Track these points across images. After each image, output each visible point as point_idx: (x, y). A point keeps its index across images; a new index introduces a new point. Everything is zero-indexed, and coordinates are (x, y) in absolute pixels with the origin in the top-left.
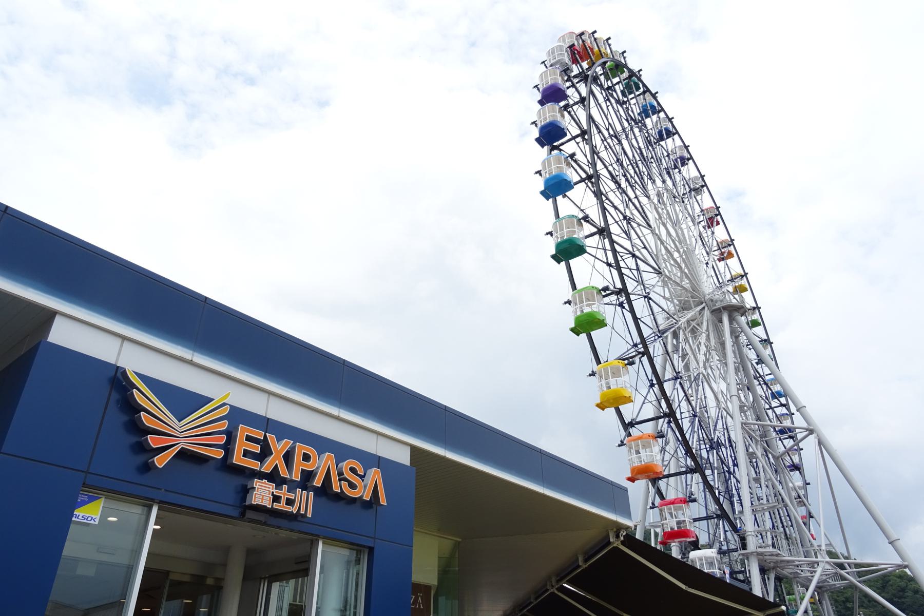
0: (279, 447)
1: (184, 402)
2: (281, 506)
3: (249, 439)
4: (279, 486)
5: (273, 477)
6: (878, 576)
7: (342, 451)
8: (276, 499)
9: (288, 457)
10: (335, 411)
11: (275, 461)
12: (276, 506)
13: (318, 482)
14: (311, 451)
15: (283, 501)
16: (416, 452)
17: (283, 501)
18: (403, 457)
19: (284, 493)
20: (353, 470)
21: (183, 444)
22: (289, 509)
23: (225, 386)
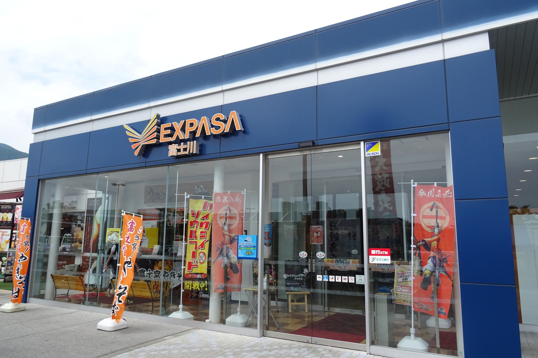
0: (178, 126)
1: (138, 127)
2: (182, 153)
3: (166, 129)
4: (179, 144)
5: (178, 141)
6: (328, 241)
7: (208, 112)
8: (179, 150)
9: (183, 129)
10: (437, 37)
11: (178, 133)
12: (179, 154)
13: (198, 135)
14: (194, 121)
15: (182, 150)
16: (493, 34)
17: (182, 150)
18: (482, 44)
19: (182, 146)
20: (218, 119)
21: (143, 143)
22: (185, 153)
23: (146, 112)
